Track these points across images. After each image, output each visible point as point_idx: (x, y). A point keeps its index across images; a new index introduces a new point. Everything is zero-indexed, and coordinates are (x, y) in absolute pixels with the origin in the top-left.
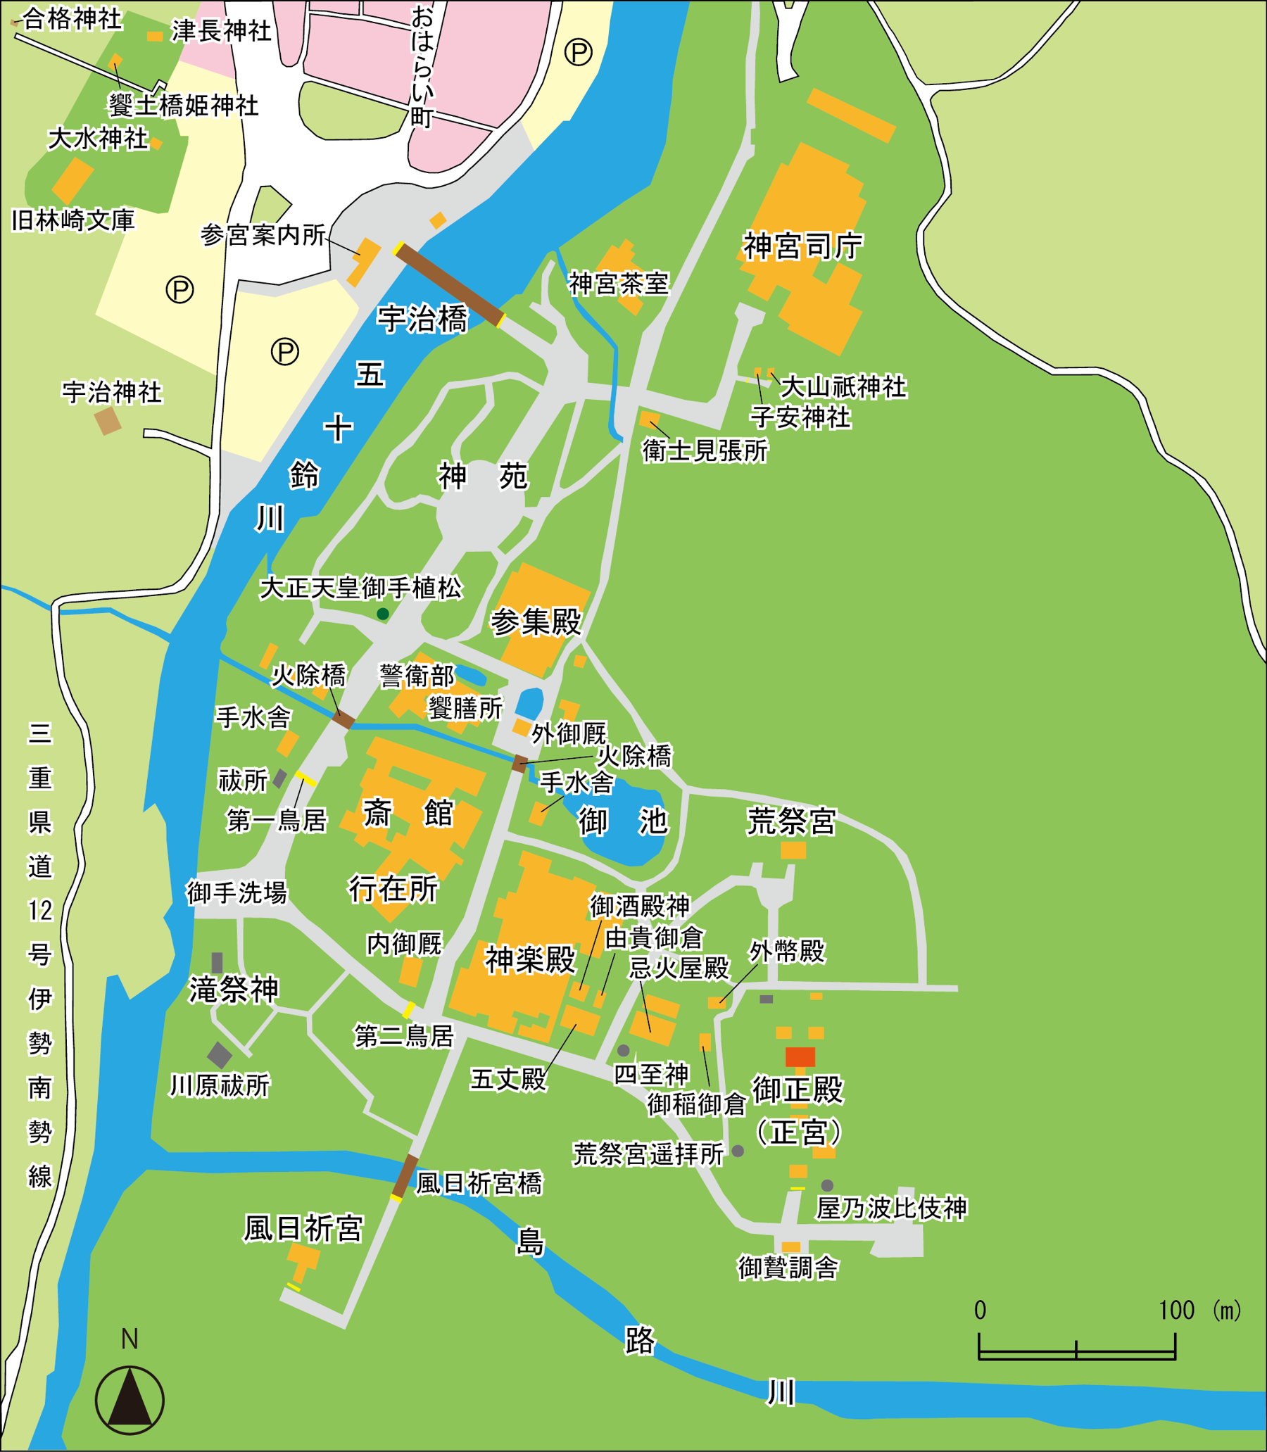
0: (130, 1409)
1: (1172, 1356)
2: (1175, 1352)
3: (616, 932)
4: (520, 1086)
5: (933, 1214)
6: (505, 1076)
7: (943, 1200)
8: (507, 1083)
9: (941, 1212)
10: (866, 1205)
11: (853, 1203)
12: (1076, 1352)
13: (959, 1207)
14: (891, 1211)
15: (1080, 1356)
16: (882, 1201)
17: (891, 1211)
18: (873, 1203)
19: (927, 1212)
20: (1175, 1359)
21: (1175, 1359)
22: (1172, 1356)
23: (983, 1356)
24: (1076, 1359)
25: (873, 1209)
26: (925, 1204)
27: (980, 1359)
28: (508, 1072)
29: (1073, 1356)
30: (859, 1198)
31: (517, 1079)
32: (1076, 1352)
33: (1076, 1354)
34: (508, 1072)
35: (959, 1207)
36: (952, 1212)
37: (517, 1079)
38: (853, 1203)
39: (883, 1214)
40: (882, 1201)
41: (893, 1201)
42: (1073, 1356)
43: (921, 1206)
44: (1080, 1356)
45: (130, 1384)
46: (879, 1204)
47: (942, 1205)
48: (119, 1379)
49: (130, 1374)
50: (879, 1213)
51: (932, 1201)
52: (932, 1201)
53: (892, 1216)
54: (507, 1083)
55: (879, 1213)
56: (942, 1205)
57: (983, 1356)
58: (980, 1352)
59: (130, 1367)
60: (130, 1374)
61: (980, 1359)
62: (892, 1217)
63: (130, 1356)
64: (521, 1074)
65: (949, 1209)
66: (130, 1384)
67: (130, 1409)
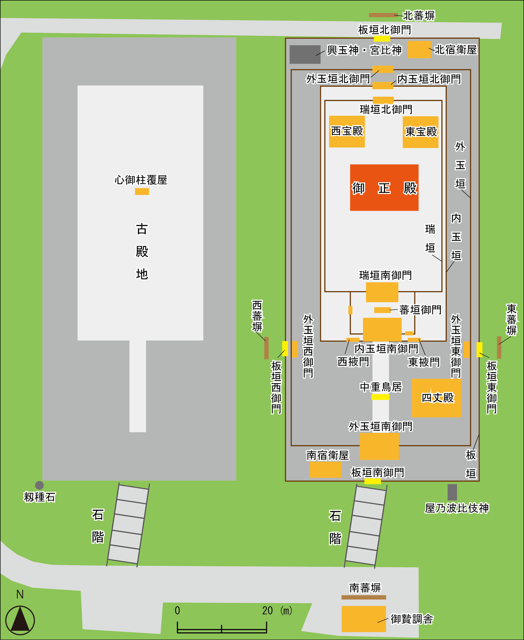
0: (20, 624)
1: (265, 631)
2: (266, 630)
3: (365, 384)
4: (443, 401)
5: (474, 510)
6: (437, 396)
7: (478, 505)
8: (437, 399)
9: (478, 510)
10: (446, 507)
11: (441, 506)
12: (222, 630)
13: (486, 508)
14: (457, 510)
15: (223, 631)
16: (453, 505)
17: (457, 510)
18: (449, 506)
19: (472, 510)
20: (266, 633)
21: (266, 633)
22: (265, 631)
23: (179, 631)
24: (222, 633)
25: (449, 508)
26: (471, 507)
27: (178, 633)
28: (438, 395)
29: (220, 631)
30: (443, 504)
31: (441, 398)
32: (222, 630)
33: (222, 630)
34: (438, 395)
35: (486, 508)
36: (482, 510)
37: (441, 398)
38: (441, 506)
39: (453, 510)
40: (453, 505)
41: (457, 505)
42: (220, 631)
43: (470, 507)
44: (223, 631)
45: (20, 613)
46: (452, 506)
47: (478, 507)
48: (16, 611)
49: (20, 610)
50: (451, 510)
51: (474, 505)
52: (474, 505)
53: (457, 511)
54: (437, 399)
55: (451, 510)
56: (478, 507)
57: (179, 631)
58: (178, 630)
59: (20, 606)
60: (20, 610)
61: (178, 633)
62: (457, 512)
63: (20, 602)
64: (443, 395)
65: (481, 508)
66: (20, 613)
67: (20, 624)
